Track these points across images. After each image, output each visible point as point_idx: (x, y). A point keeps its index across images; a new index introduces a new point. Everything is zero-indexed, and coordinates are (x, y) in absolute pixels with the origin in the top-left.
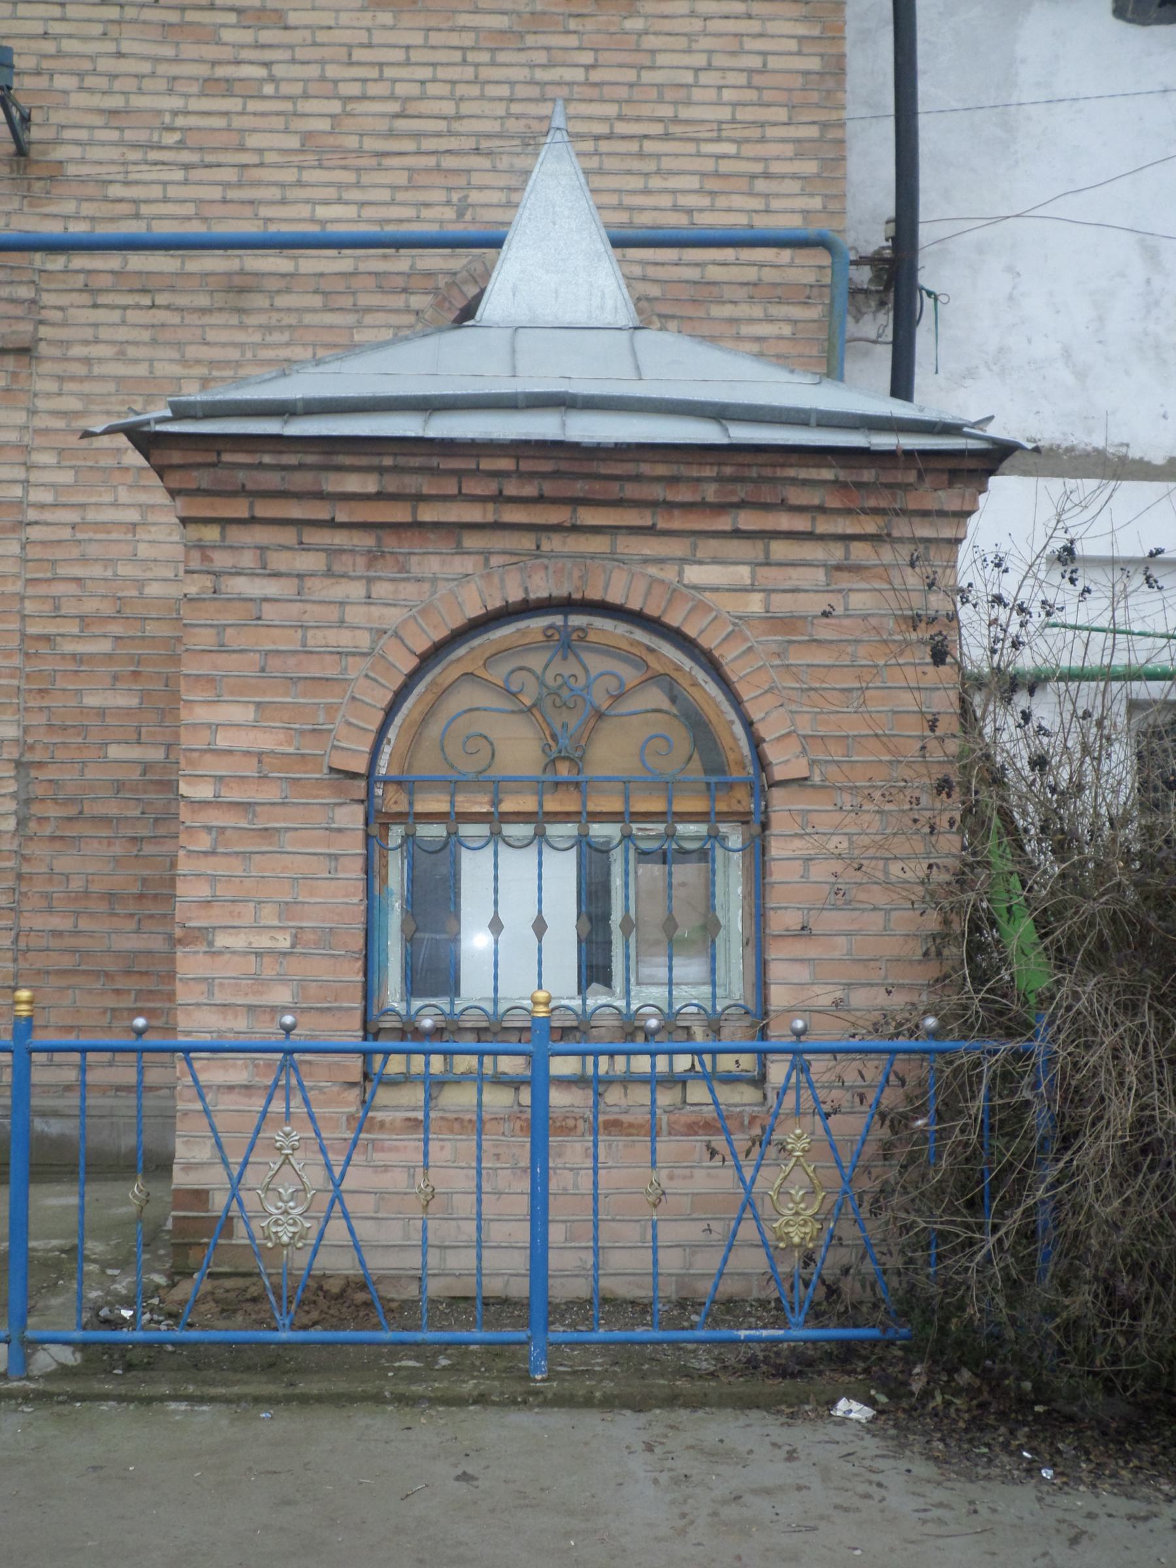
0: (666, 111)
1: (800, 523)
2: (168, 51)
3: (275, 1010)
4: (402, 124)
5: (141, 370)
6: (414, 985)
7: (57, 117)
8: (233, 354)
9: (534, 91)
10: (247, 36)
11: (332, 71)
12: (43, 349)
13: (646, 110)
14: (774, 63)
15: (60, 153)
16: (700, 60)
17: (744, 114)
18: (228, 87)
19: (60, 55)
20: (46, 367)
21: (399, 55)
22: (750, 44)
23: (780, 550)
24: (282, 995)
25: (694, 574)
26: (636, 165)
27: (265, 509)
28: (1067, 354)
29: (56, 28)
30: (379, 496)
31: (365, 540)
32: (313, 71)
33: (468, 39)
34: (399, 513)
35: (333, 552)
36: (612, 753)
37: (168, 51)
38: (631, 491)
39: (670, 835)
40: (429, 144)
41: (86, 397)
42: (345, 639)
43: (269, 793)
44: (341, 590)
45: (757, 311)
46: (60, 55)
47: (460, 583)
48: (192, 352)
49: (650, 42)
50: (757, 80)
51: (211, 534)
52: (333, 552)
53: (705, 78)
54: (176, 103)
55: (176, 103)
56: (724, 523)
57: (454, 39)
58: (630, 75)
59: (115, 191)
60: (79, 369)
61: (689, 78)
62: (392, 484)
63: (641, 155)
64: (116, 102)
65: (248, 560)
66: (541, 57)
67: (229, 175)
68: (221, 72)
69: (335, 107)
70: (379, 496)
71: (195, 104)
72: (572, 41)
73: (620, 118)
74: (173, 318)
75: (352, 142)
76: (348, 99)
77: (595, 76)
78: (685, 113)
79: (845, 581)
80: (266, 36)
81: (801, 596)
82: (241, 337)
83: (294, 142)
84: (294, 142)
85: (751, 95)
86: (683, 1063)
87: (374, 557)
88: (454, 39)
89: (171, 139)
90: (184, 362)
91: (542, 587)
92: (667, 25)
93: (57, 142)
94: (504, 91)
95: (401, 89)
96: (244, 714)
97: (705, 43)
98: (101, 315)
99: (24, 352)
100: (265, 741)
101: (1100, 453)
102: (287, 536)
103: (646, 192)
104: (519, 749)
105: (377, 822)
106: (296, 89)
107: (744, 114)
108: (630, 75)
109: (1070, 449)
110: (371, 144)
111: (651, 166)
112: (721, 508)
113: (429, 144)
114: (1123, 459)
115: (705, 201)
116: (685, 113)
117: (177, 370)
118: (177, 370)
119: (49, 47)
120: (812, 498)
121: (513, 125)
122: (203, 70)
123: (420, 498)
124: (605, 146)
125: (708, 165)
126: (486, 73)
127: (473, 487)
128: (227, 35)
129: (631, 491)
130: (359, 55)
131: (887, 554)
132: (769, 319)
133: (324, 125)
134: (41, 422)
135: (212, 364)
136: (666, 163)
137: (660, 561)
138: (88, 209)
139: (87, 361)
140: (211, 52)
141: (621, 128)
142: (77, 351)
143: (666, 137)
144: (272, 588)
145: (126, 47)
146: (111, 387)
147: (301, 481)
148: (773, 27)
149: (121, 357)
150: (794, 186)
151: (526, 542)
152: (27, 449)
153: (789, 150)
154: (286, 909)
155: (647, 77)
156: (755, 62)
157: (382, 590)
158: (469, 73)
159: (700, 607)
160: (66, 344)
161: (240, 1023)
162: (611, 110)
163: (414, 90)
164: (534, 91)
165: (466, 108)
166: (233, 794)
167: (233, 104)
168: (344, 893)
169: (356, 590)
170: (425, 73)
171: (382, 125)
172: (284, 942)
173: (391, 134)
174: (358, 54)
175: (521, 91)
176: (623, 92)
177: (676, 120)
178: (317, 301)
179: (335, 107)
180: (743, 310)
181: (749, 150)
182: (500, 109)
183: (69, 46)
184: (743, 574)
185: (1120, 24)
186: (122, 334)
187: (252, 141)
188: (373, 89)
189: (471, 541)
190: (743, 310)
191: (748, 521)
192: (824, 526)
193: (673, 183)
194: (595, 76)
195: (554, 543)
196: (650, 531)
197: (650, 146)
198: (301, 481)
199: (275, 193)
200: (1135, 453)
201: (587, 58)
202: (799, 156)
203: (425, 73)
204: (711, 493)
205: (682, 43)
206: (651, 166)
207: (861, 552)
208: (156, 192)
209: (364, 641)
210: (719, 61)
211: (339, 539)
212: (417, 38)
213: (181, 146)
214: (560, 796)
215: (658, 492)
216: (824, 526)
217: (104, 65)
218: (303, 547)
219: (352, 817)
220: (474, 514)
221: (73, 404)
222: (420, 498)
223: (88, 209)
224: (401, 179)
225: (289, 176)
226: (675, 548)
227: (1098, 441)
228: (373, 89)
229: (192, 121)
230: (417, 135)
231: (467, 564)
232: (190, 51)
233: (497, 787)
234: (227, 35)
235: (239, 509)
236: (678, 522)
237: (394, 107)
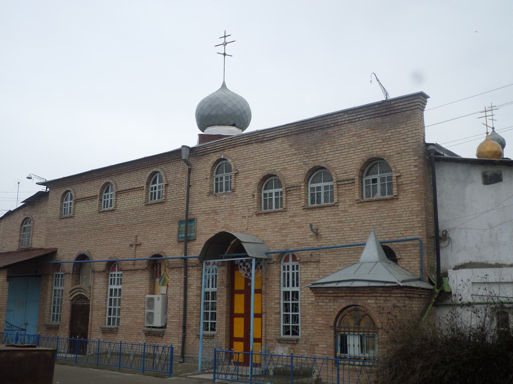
0: (399, 219)
1: (380, 295)
2: (334, 218)
3: (325, 354)
4: (363, 225)
5: (332, 263)
6: (342, 352)
7: (321, 229)
8: (343, 260)
9: (380, 218)
10: (343, 214)
11: (354, 218)
12: (321, 261)
13: (396, 219)
14: (414, 209)
15: (321, 234)
16: (403, 210)
17: (410, 218)
18: (341, 222)
19: (321, 220)
20: (321, 264)
21: (362, 215)
22: (410, 207)
23: (378, 298)
24: (326, 353)
25: (369, 301)
26: (395, 227)
27: (322, 295)
28: (476, 246)
29: (320, 216)
30: (333, 293)
31: (333, 298)
32: (351, 218)
33: (371, 211)
34: (336, 295)
35: (330, 300)
36: (363, 324)
37: (334, 218)
38: (360, 292)
39: (368, 334)
40: (367, 227)
41: (326, 268)
42: (331, 310)
43: (324, 328)
44: (330, 304)
45: (413, 249)
46: (321, 220)
47: (343, 303)
48: (338, 260)
49: (396, 208)
50: (412, 212)
51: (317, 298)
52: (330, 300)
53: (404, 213)
54: (335, 225)
55: (335, 225)
56: (371, 295)
57: (369, 211)
58: (393, 214)
59: (328, 238)
60: (325, 264)
61: (402, 213)
62: (334, 292)
63: (395, 226)
64: (327, 226)
65: (321, 301)
66: (381, 212)
67: (342, 235)
68: (340, 220)
69: (354, 223)
70: (333, 293)
71: (337, 225)
72: (385, 209)
73: (392, 220)
74: (336, 256)
75: (357, 228)
76: (356, 222)
77: (389, 214)
78: (401, 219)
79: (387, 302)
80: (346, 214)
81: (505, 270)
82: (344, 258)
83: (349, 229)
84: (349, 229)
85: (411, 215)
86: (371, 364)
87: (334, 300)
88: (369, 211)
89: (334, 230)
90: (337, 262)
91: (351, 303)
92: (398, 205)
93: (321, 232)
94: (376, 218)
95: (363, 220)
96: (321, 319)
97: (404, 207)
98: (327, 256)
99: (318, 262)
100: (323, 322)
101: (483, 263)
102: (325, 298)
103: (397, 231)
104: (352, 323)
105: (336, 332)
106: (349, 221)
107: (410, 218)
108: (393, 214)
109: (478, 263)
110: (359, 228)
111: (397, 227)
112: (371, 293)
113: (367, 227)
114: (487, 264)
115: (405, 232)
116: (401, 219)
117: (337, 263)
118: (337, 263)
119: (320, 219)
120: (380, 292)
121: (378, 223)
122: (338, 220)
123: (337, 293)
124: (390, 225)
125: (405, 226)
126: (374, 216)
127: (343, 292)
128: (341, 214)
129: (360, 292)
130: (357, 215)
131: (392, 298)
132: (415, 250)
133: (353, 226)
134: (321, 271)
135: (341, 262)
136: (399, 227)
137: (365, 300)
138: (325, 241)
139: (326, 262)
140: (339, 217)
141: (392, 222)
142: (325, 261)
143: (399, 223)
144: (323, 304)
145: (329, 218)
146: (328, 266)
147: (325, 292)
148: (413, 204)
149: (330, 262)
150: (418, 228)
151: (350, 298)
152: (319, 275)
153: (417, 222)
154: (326, 342)
155: (396, 214)
156: (411, 209)
157: (335, 304)
158: (371, 216)
159: (369, 305)
160: (323, 260)
161: (322, 356)
162: (391, 219)
163: (364, 219)
164: (380, 218)
165: (372, 221)
166: (320, 328)
167: (342, 224)
168: (331, 341)
169: (332, 304)
170: (366, 217)
171: (361, 225)
172: (326, 346)
173: (362, 227)
174: (357, 215)
175: (379, 218)
176: (393, 216)
177: (400, 220)
178: (353, 252)
179: (354, 223)
180: (411, 249)
181: (411, 223)
182: (376, 221)
183: (322, 218)
184: (374, 301)
185: (486, 186)
186: (330, 258)
187: (345, 229)
188: (359, 220)
189: (344, 298)
190: (411, 249)
191: (374, 295)
192: (383, 295)
193: (400, 230)
194: (389, 214)
195: (353, 298)
196: (363, 296)
197: (397, 224)
198: (325, 292)
199: (347, 237)
200: (489, 263)
201: (387, 212)
202: (418, 223)
203: (366, 217)
204: (369, 291)
205: (400, 208)
206: (397, 227)
207: (388, 298)
208: (333, 238)
209: (333, 310)
210: (406, 210)
211: (330, 298)
212: (364, 212)
213: (336, 231)
214: (357, 329)
215: (363, 292)
216: (383, 295)
217: (326, 221)
218: (326, 299)
219: (332, 331)
220: (343, 295)
221: (324, 269)
222: (337, 293)
223: (325, 241)
224: (363, 233)
225: (349, 234)
226: (366, 298)
227: (483, 261)
228: (359, 220)
229: (337, 227)
230: (365, 226)
231: (344, 301)
232: (336, 217)
233: (349, 328)
234: (341, 214)
235: (320, 295)
236: (366, 295)
237: (362, 223)
